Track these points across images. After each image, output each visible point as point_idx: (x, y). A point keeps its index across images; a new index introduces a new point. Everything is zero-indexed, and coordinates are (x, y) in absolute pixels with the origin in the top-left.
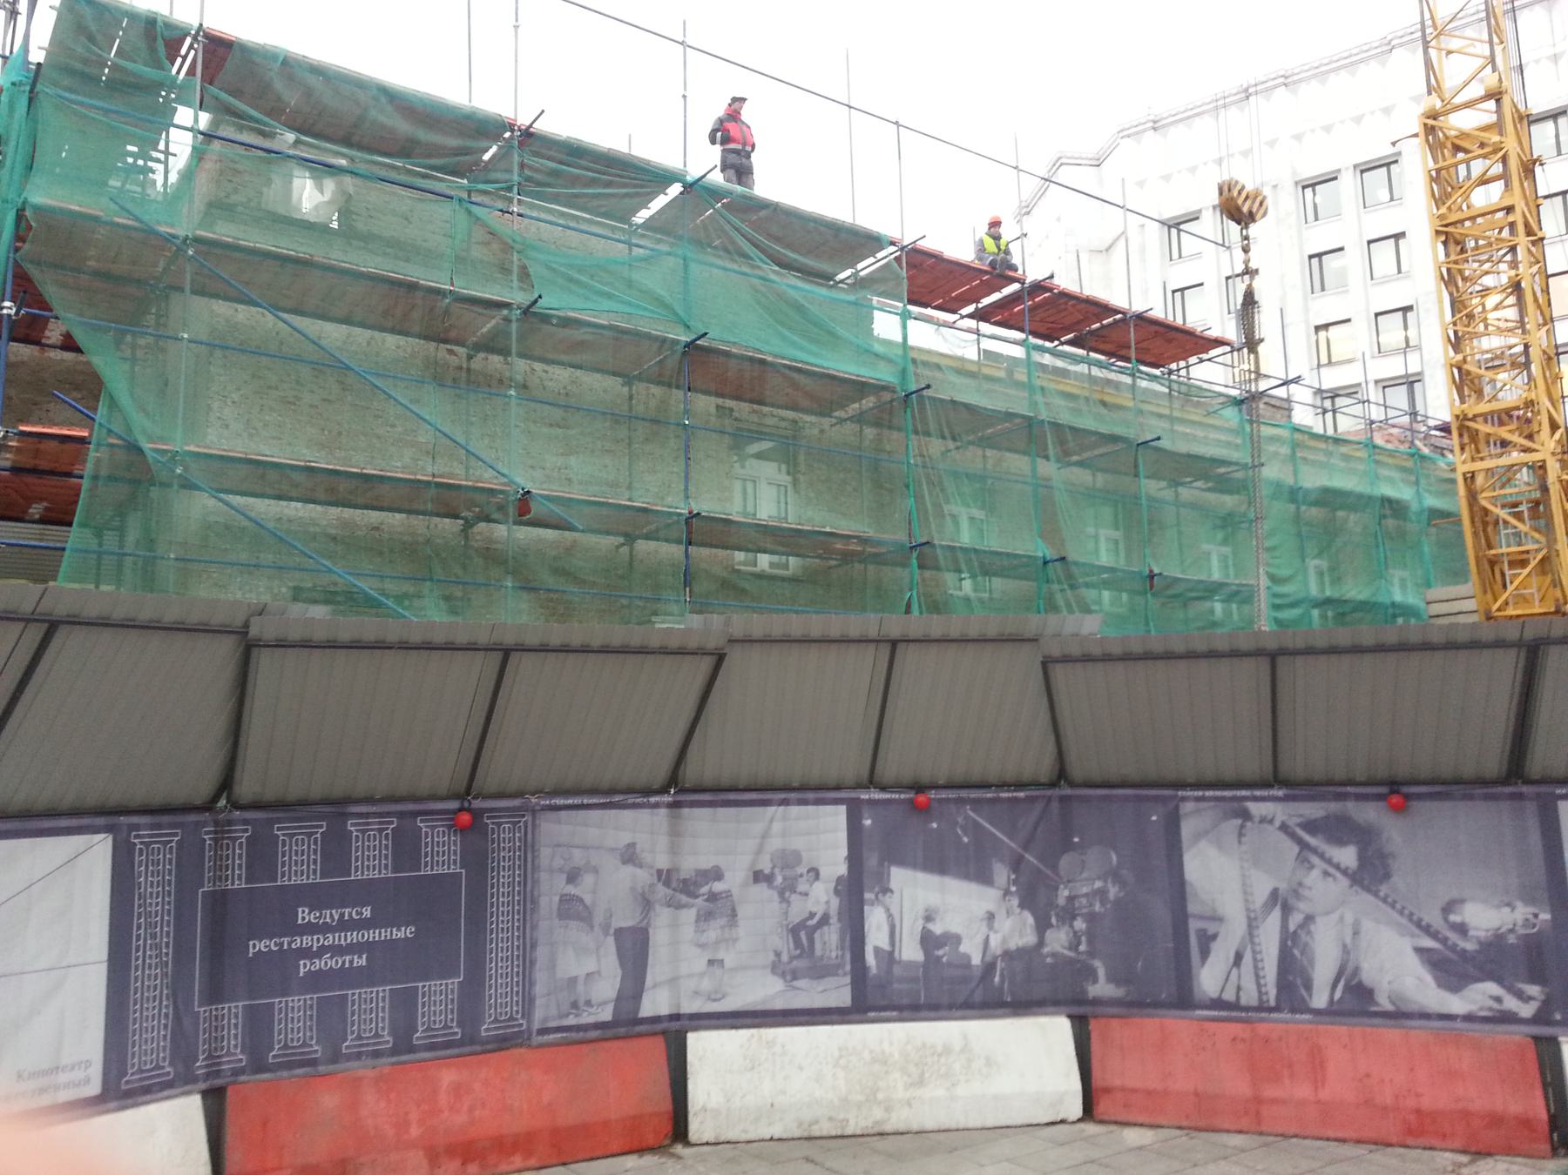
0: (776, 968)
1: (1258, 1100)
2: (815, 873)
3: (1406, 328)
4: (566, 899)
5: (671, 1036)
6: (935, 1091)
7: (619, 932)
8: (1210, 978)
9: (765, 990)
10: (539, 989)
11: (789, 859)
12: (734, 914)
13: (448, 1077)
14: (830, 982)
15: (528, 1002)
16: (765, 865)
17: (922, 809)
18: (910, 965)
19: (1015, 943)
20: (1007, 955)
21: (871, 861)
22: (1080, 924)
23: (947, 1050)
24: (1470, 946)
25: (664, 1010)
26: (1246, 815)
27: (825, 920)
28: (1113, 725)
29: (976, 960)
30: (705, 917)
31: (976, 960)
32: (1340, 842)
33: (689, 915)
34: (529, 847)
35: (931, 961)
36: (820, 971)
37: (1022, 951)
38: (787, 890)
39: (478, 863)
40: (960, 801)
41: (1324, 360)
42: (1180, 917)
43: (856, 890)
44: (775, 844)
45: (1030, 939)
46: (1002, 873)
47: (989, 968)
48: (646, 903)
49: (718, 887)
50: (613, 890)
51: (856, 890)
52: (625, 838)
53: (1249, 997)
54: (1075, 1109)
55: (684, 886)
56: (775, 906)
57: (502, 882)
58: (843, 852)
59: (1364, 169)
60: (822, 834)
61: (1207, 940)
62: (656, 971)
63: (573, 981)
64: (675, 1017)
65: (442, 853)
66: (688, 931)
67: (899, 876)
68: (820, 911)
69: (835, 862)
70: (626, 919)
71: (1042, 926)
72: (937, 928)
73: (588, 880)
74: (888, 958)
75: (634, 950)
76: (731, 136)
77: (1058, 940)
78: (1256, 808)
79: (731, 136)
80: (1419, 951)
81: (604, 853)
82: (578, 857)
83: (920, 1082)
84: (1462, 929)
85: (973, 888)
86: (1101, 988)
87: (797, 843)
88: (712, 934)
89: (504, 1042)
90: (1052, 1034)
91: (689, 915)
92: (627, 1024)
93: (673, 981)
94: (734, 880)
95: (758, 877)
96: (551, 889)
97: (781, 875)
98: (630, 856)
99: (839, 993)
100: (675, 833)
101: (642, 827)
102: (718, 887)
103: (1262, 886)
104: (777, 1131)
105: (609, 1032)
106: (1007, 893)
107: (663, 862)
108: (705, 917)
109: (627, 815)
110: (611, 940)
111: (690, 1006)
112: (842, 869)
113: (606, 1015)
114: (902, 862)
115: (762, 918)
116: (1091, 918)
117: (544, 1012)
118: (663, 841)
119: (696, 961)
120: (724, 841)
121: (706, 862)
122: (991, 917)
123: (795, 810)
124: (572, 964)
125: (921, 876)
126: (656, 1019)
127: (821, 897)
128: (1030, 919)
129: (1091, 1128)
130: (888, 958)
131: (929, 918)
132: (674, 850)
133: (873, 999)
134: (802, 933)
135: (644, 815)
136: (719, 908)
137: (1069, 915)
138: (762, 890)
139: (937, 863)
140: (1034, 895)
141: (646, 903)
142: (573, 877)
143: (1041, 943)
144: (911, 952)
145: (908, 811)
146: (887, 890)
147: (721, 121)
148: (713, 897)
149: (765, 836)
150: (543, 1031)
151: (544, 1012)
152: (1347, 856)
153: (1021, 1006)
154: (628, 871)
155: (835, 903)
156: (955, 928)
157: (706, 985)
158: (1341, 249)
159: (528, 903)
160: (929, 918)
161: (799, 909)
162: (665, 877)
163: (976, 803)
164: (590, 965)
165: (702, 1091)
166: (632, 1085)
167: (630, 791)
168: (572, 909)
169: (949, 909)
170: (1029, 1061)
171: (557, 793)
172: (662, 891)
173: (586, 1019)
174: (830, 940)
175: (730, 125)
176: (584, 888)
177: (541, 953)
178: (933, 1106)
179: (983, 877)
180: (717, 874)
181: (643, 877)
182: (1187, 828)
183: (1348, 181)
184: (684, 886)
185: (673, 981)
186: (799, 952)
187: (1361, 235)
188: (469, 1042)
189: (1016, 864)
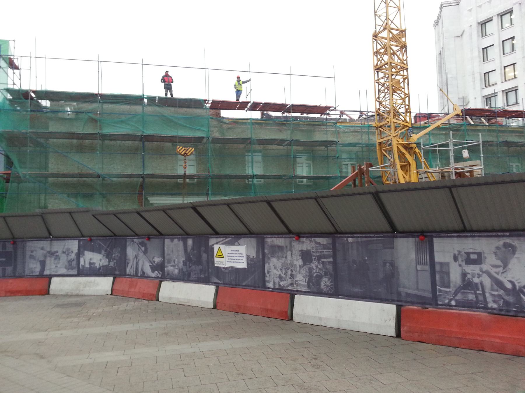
0: (66, 268)
1: (128, 291)
2: (72, 252)
3: (514, 71)
4: (31, 255)
5: (50, 278)
6: (87, 288)
7: (40, 261)
8: (128, 271)
9: (63, 271)
10: (26, 269)
11: (68, 249)
12: (59, 259)
13: (10, 281)
14: (74, 270)
15: (24, 271)
16: (65, 250)
17: (91, 240)
18: (87, 268)
19: (105, 264)
20: (103, 266)
21: (82, 250)
22: (115, 261)
23: (91, 282)
24: (155, 265)
25: (48, 274)
26: (133, 241)
27: (74, 260)
28: (118, 227)
29: (98, 267)
30: (55, 259)
31: (98, 267)
32: (143, 246)
33: (53, 259)
34: (24, 247)
35: (90, 267)
36: (72, 268)
37: (106, 266)
38: (68, 255)
39: (15, 249)
40: (97, 239)
41: (487, 85)
42: (126, 259)
43: (79, 254)
44: (66, 247)
45: (107, 263)
46: (103, 252)
47: (100, 268)
48: (45, 256)
49: (57, 254)
50: (39, 254)
51: (79, 254)
52: (42, 246)
53: (132, 274)
54: (110, 293)
55: (52, 254)
56: (66, 258)
57: (19, 251)
58: (77, 248)
59: (501, 15)
60: (74, 245)
61: (128, 263)
62: (47, 267)
63: (32, 268)
64: (50, 275)
65: (10, 248)
66: (53, 261)
67: (86, 253)
68: (73, 258)
69: (75, 249)
70: (42, 259)
71: (109, 261)
72: (92, 261)
73: (35, 252)
74: (83, 266)
75: (43, 264)
76: (167, 81)
77: (112, 264)
78: (135, 240)
79: (167, 81)
80: (150, 266)
81: (38, 248)
82: (33, 249)
83: (85, 287)
84: (154, 262)
85: (98, 255)
86: (117, 273)
87: (70, 247)
88: (56, 262)
89: (21, 277)
90: (110, 280)
91: (53, 259)
92: (41, 276)
93: (50, 269)
94: (59, 253)
95: (64, 252)
96: (28, 254)
97: (67, 252)
98: (42, 249)
99: (75, 272)
100: (51, 245)
101: (45, 244)
102: (57, 254)
103: (135, 254)
104: (62, 293)
105: (38, 277)
106: (104, 255)
107: (48, 250)
108: (55, 259)
109: (42, 242)
110: (39, 263)
111: (53, 273)
112: (77, 251)
113: (38, 274)
114: (87, 250)
115: (64, 259)
116: (117, 260)
117: (27, 272)
118: (49, 246)
119: (53, 266)
120: (58, 246)
121: (55, 250)
122: (101, 260)
123: (70, 241)
124: (32, 266)
125: (90, 253)
126: (46, 275)
127: (73, 256)
128: (107, 260)
129: (112, 296)
130: (83, 266)
131: (90, 260)
132: (51, 248)
133: (81, 273)
134: (70, 262)
135: (45, 242)
136: (57, 258)
137: (113, 260)
138: (64, 255)
139: (93, 250)
140: (108, 256)
141: (45, 256)
142: (32, 252)
143: (109, 264)
144: (87, 265)
145: (88, 242)
146: (84, 255)
147: (163, 77)
148: (56, 256)
149: (65, 246)
150: (27, 276)
151: (27, 272)
152: (143, 249)
153: (105, 275)
154: (42, 251)
155: (75, 257)
156: (95, 262)
157: (55, 270)
158: (493, 45)
159: (24, 255)
160: (90, 260)
161: (70, 258)
162: (49, 252)
163: (100, 239)
164: (35, 266)
165: (52, 287)
166: (39, 285)
167: (43, 238)
168: (32, 257)
169: (94, 258)
170: (104, 284)
171: (29, 238)
172: (48, 255)
173: (34, 274)
174: (74, 263)
175: (166, 78)
176: (34, 254)
177: (26, 264)
178: (87, 291)
179: (100, 253)
180: (57, 252)
181: (45, 252)
182: (128, 243)
183: (495, 19)
184: (52, 254)
185: (50, 269)
186: (69, 266)
187: (499, 39)
188: (14, 276)
189: (106, 251)
